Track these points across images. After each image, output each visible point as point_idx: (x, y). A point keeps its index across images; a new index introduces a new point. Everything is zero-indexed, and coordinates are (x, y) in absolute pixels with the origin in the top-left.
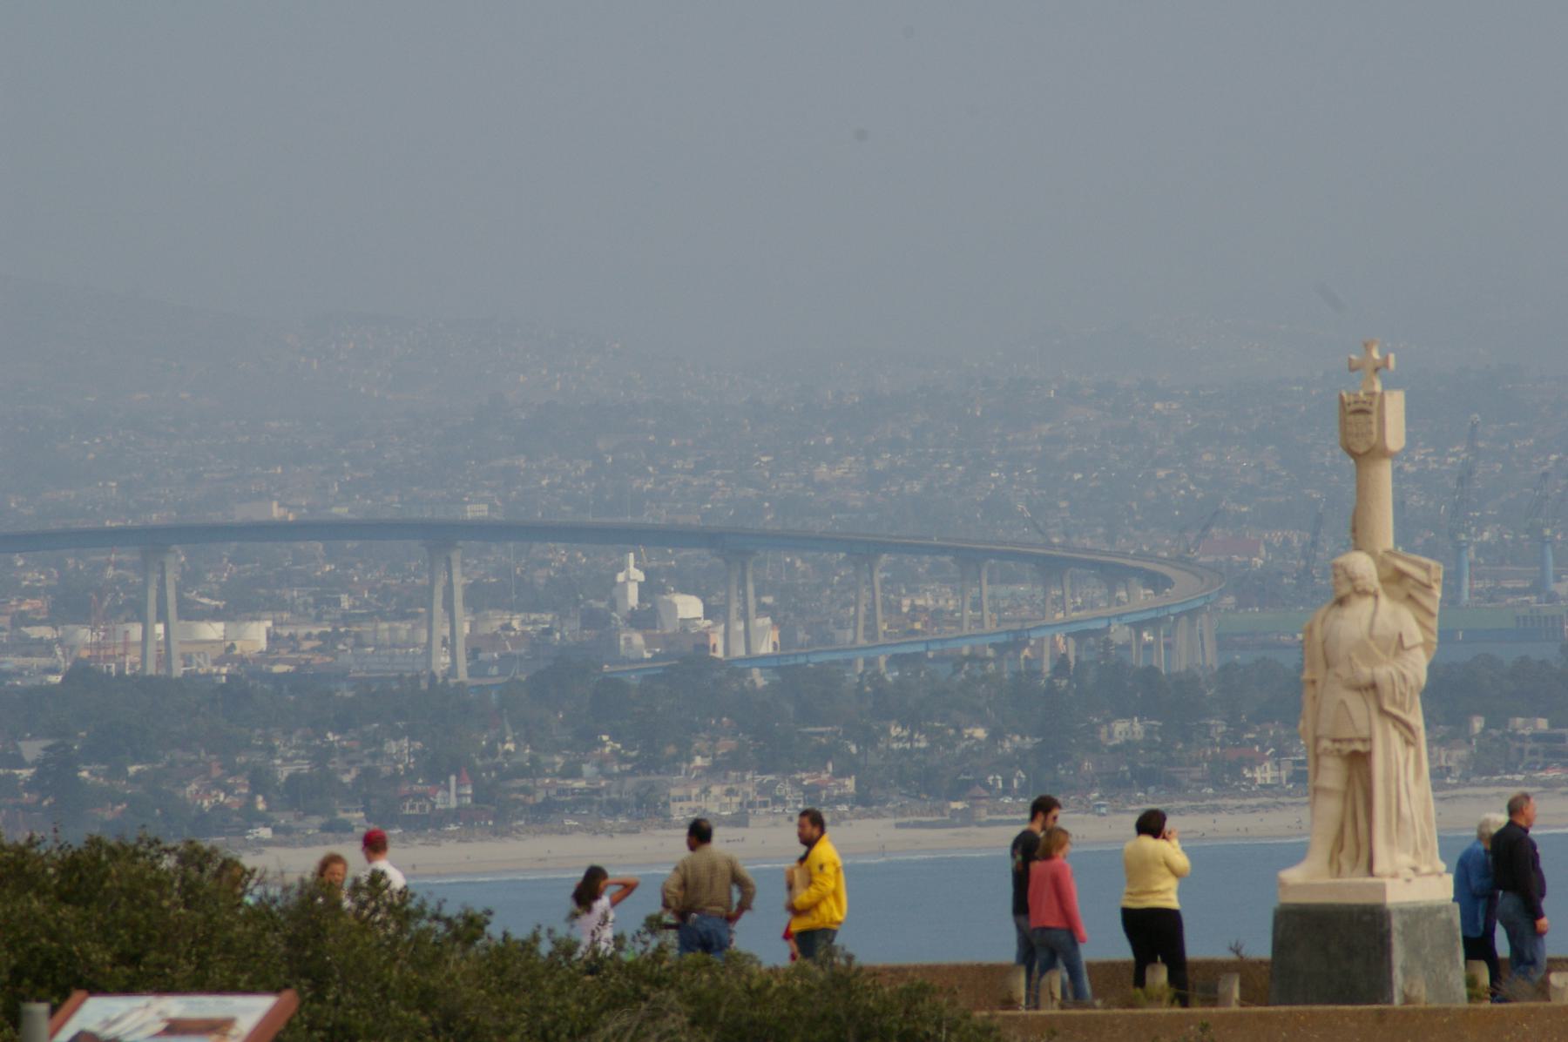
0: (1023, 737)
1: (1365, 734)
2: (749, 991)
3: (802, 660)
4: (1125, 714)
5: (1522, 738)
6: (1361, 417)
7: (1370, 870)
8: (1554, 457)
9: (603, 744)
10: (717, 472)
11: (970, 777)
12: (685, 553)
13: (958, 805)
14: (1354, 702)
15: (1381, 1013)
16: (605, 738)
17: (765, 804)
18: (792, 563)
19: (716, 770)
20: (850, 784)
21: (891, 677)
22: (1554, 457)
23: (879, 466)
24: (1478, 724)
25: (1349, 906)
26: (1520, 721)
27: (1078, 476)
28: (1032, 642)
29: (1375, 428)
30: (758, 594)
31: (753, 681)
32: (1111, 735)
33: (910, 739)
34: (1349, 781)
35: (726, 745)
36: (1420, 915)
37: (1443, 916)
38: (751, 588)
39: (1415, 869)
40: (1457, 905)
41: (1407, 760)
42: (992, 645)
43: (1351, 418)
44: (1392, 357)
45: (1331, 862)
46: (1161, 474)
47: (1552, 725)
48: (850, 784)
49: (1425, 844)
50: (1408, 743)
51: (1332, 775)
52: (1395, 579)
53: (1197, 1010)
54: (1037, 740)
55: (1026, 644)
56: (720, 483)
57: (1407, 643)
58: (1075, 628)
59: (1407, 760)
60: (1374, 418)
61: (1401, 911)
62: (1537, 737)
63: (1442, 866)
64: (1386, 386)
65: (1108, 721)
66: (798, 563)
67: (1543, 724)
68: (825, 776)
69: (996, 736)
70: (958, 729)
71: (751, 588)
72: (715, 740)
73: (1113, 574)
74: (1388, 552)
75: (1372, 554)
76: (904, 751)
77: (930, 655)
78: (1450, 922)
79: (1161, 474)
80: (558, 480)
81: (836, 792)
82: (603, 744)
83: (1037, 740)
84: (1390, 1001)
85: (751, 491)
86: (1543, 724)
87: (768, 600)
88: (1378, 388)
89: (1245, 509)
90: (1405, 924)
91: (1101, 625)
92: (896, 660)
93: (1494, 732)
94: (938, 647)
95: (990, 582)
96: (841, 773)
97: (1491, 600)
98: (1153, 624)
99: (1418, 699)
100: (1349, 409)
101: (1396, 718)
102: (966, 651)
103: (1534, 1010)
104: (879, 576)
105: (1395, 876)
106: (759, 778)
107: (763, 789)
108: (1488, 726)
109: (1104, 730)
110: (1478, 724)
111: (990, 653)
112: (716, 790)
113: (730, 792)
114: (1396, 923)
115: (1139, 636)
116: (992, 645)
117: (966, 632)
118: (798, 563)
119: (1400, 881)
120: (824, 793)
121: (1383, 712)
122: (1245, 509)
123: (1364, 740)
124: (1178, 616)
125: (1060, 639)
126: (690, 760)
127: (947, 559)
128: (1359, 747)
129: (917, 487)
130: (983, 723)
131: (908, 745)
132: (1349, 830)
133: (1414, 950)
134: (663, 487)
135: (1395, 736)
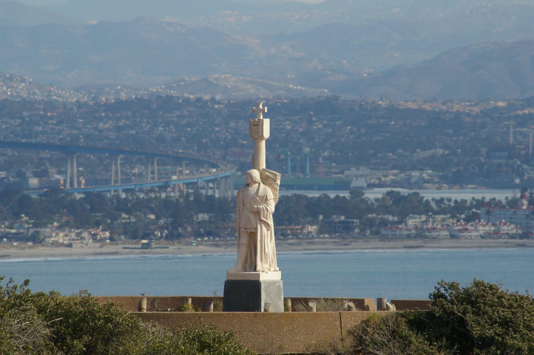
0: (167, 218)
1: (255, 226)
2: (57, 305)
3: (92, 190)
4: (201, 212)
5: (336, 223)
6: (256, 127)
7: (255, 270)
8: (349, 128)
9: (22, 218)
10: (65, 125)
11: (149, 232)
12: (52, 153)
13: (145, 241)
14: (252, 216)
15: (256, 314)
16: (23, 215)
17: (78, 240)
18: (89, 157)
19: (61, 228)
20: (107, 234)
21: (123, 196)
22: (349, 128)
23: (121, 124)
24: (321, 217)
25: (248, 280)
26: (335, 216)
27: (189, 129)
28: (171, 186)
29: (260, 130)
30: (78, 167)
31: (75, 197)
32: (197, 219)
33: (129, 218)
34: (249, 242)
35: (65, 219)
36: (271, 284)
37: (277, 284)
38: (75, 165)
39: (269, 270)
40: (282, 281)
41: (268, 235)
42: (157, 187)
43: (253, 127)
44: (266, 108)
45: (243, 266)
46: (217, 129)
47: (346, 218)
48: (107, 234)
49: (272, 262)
50: (268, 230)
51: (244, 240)
52: (265, 179)
53: (200, 312)
54: (173, 219)
55: (169, 187)
56: (65, 128)
57: (268, 198)
58: (186, 181)
59: (268, 235)
60: (260, 127)
61: (264, 283)
62: (341, 222)
63: (278, 269)
64: (264, 117)
65: (197, 214)
66: (92, 157)
67: (343, 218)
68: (99, 230)
69: (158, 218)
70: (145, 215)
71: (75, 165)
72: (61, 217)
73: (197, 163)
74: (263, 169)
75: (259, 170)
76: (126, 223)
77: (137, 189)
78: (279, 286)
79: (217, 129)
80: (8, 126)
81: (102, 236)
82: (22, 218)
83: (173, 219)
84: (260, 311)
85: (75, 132)
86: (343, 218)
87: (81, 169)
88: (261, 118)
89: (245, 142)
90: (265, 287)
91: (195, 180)
92: (126, 191)
93: (327, 220)
94: (139, 187)
95: (158, 165)
96: (104, 230)
97: (327, 175)
98: (213, 181)
99: (271, 216)
100: (252, 124)
101: (265, 222)
102: (149, 188)
103: (303, 314)
104: (119, 162)
105: (263, 271)
106: (76, 231)
107: (78, 235)
108: (324, 218)
109: (195, 217)
110: (321, 217)
111: (156, 189)
112: (61, 234)
113: (66, 235)
114: (263, 286)
115: (208, 185)
116: (157, 187)
117: (149, 182)
118: (92, 157)
119: (264, 273)
120: (99, 236)
121: (261, 220)
122: (245, 142)
123: (254, 229)
124: (221, 178)
125: (181, 184)
126: (52, 224)
127: (143, 157)
128: (253, 230)
129: (134, 132)
130: (153, 212)
131: (128, 221)
132: (249, 257)
133: (268, 294)
134: (45, 130)
135: (264, 228)
